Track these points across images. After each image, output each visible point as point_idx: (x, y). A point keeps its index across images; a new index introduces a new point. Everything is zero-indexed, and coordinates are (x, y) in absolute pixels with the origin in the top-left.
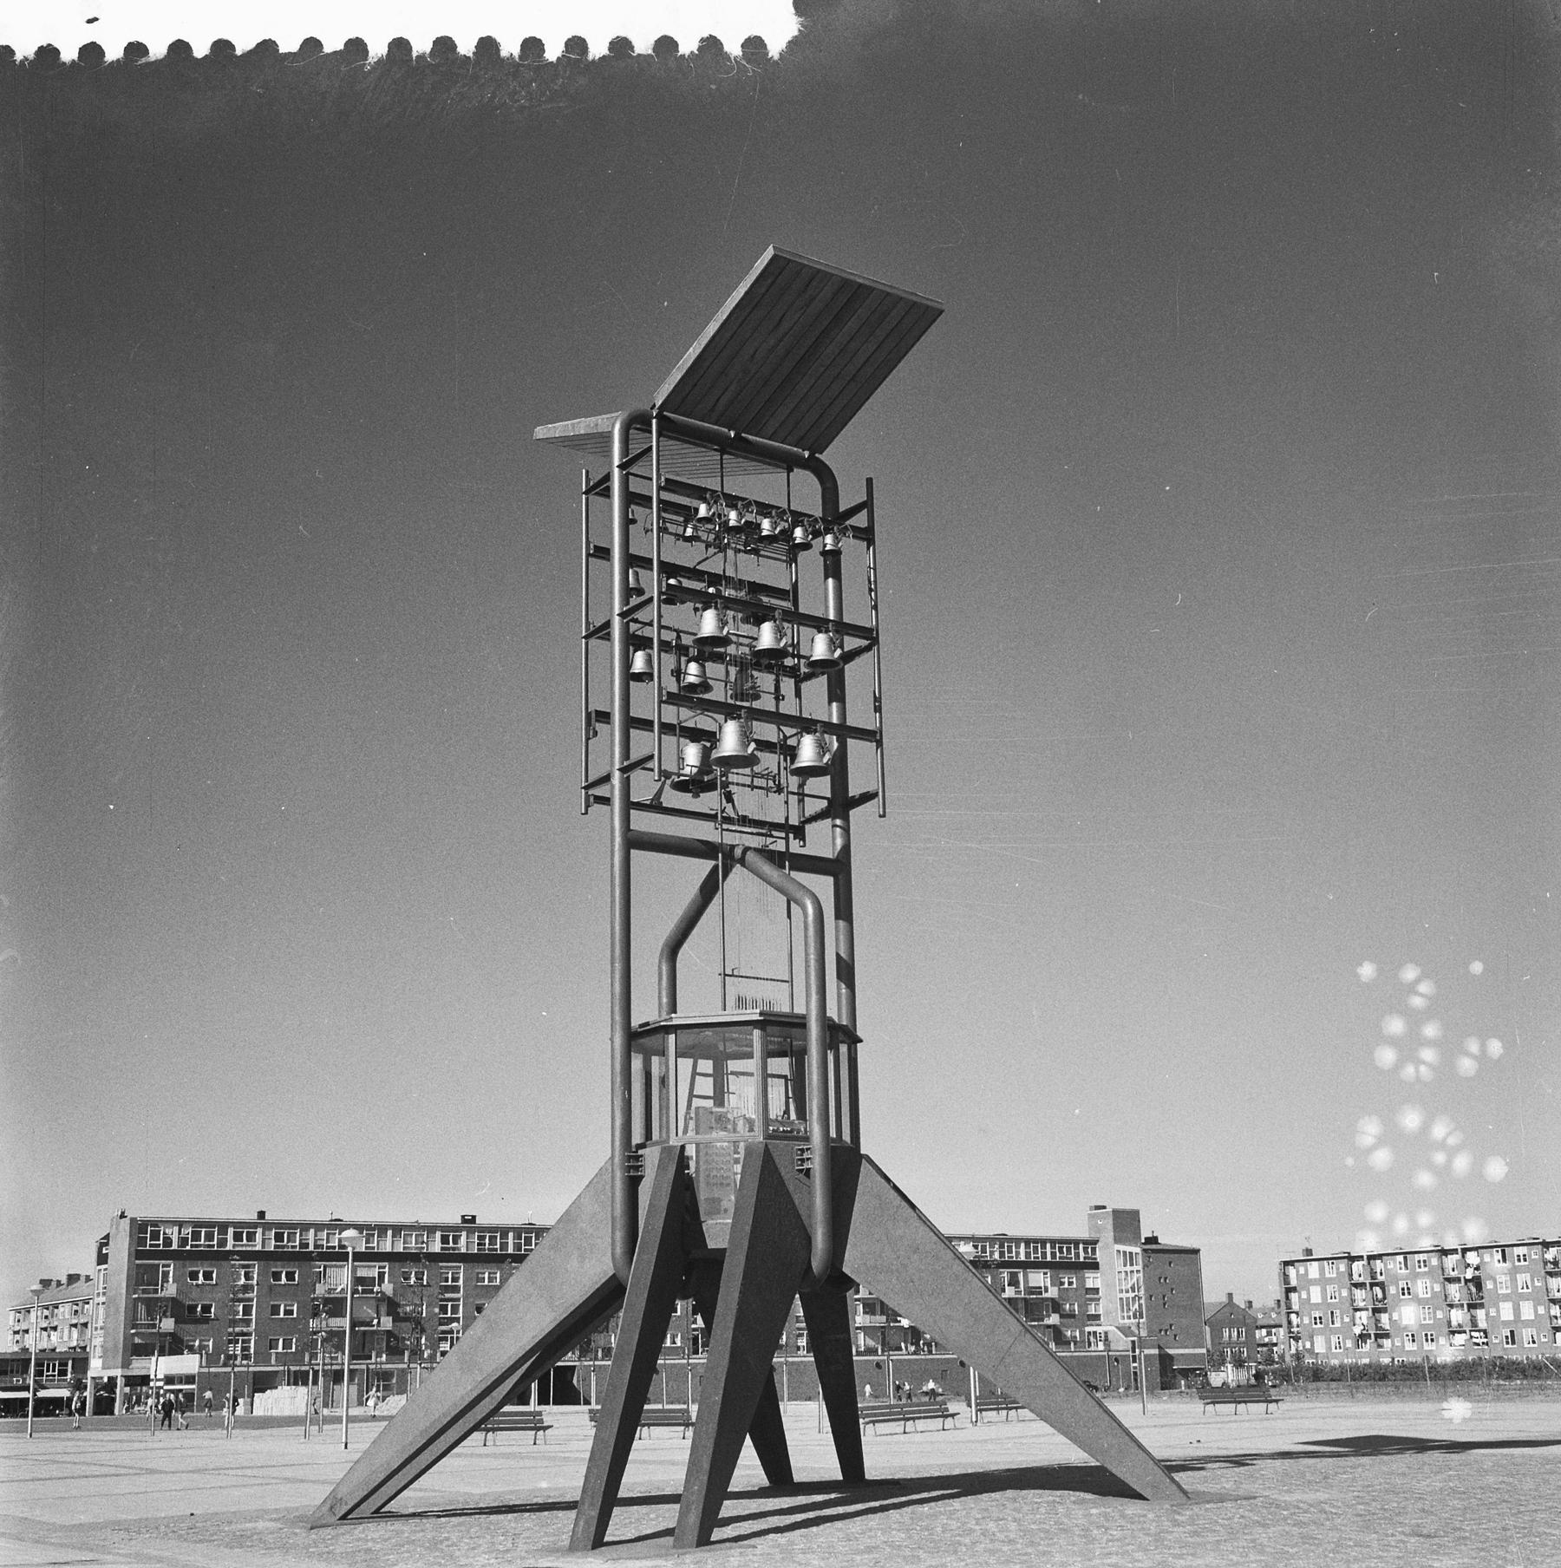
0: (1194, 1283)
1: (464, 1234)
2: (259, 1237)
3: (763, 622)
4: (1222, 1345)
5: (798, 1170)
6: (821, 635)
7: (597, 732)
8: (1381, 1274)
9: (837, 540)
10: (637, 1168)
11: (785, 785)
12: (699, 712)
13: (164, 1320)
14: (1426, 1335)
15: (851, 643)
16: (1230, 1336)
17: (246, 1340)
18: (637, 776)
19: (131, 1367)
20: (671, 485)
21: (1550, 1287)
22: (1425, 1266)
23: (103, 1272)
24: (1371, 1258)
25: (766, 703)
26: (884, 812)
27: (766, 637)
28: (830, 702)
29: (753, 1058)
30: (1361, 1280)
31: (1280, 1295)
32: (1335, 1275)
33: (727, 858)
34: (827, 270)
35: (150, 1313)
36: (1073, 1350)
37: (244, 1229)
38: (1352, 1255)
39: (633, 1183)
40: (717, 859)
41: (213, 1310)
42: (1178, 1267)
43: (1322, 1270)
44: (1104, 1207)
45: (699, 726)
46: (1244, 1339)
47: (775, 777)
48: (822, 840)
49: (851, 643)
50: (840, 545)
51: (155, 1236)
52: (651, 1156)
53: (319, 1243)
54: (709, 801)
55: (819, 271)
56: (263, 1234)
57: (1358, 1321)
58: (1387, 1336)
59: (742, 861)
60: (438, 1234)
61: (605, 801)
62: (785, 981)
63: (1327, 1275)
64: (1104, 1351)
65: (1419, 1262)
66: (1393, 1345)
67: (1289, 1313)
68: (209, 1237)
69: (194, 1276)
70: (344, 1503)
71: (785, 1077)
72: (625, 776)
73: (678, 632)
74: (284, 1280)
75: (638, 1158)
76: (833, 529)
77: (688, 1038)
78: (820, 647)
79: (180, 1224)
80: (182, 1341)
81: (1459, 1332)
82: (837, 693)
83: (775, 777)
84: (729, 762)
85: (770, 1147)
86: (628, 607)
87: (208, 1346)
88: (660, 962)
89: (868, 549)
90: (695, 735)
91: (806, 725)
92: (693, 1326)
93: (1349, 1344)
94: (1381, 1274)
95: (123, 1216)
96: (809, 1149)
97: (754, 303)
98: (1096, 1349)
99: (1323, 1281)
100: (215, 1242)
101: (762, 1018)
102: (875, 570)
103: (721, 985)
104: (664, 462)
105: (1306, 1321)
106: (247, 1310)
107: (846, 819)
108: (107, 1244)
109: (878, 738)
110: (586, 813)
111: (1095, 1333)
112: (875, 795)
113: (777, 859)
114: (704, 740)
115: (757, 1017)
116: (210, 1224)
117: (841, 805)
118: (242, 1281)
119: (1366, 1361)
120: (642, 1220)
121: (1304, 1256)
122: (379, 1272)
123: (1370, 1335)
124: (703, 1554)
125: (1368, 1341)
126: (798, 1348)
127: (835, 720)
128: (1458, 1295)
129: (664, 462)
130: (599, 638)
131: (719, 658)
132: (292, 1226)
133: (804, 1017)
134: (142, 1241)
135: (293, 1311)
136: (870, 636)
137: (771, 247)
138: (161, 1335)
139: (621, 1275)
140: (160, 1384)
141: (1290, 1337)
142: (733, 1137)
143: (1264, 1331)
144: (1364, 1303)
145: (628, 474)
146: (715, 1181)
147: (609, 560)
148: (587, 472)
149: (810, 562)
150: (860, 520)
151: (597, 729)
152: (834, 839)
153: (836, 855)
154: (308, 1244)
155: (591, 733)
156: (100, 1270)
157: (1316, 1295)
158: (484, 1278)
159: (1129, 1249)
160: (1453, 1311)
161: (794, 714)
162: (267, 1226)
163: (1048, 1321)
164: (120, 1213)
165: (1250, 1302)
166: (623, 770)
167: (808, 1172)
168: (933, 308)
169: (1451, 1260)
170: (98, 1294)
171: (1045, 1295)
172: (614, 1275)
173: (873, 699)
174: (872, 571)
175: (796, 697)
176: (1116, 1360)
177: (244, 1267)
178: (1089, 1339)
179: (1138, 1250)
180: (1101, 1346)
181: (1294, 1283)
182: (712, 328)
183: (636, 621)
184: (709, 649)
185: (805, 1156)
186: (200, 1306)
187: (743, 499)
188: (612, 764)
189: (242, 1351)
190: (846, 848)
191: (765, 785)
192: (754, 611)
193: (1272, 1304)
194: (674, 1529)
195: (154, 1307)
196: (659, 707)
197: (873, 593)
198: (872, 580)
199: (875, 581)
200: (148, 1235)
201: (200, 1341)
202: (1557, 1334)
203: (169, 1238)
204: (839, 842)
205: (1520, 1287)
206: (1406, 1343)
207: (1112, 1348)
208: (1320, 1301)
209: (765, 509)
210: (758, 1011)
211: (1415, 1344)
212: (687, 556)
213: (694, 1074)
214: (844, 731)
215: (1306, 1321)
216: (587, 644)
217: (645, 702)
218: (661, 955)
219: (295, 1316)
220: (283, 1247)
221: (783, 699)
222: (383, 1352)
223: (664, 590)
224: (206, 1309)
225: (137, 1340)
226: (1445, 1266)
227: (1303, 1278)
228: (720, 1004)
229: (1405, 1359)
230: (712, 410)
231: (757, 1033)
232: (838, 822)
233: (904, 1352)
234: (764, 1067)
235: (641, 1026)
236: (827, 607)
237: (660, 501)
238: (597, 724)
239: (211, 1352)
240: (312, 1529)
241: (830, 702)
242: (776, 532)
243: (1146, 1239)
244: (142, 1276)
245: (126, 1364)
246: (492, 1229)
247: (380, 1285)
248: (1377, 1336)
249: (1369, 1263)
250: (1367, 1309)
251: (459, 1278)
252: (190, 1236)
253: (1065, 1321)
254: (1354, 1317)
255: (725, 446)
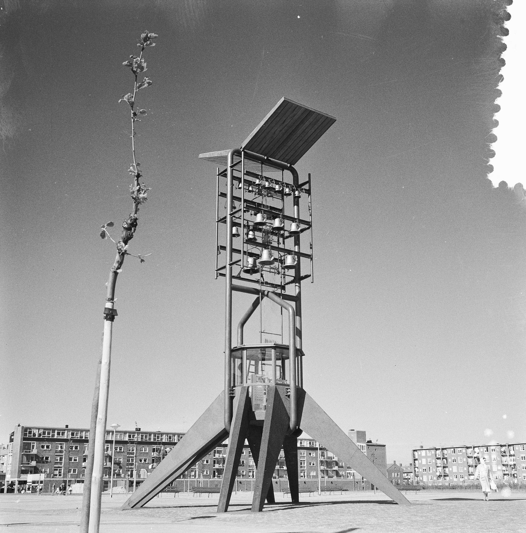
0: (384, 457)
1: (136, 434)
2: (66, 434)
3: (276, 218)
4: (392, 479)
5: (286, 395)
6: (294, 223)
7: (220, 253)
8: (446, 455)
9: (299, 193)
10: (233, 394)
11: (281, 272)
12: (254, 246)
13: (32, 462)
14: (461, 476)
15: (303, 226)
16: (394, 475)
17: (61, 469)
18: (234, 266)
19: (20, 477)
20: (248, 173)
21: (503, 460)
22: (461, 452)
23: (11, 445)
24: (443, 449)
25: (275, 244)
26: (313, 281)
27: (277, 223)
28: (295, 246)
29: (271, 360)
30: (439, 457)
31: (412, 462)
32: (431, 455)
33: (262, 294)
34: (301, 106)
35: (28, 460)
36: (342, 478)
37: (61, 431)
38: (437, 448)
39: (231, 398)
40: (259, 295)
41: (49, 459)
42: (379, 450)
43: (426, 454)
44: (354, 430)
45: (252, 252)
46: (399, 477)
47: (277, 269)
48: (291, 290)
49: (303, 226)
50: (300, 195)
51: (30, 433)
52: (238, 390)
53: (86, 436)
54: (256, 276)
55: (298, 106)
56: (67, 433)
57: (438, 471)
58: (448, 476)
59: (267, 296)
60: (128, 434)
61: (224, 275)
62: (280, 335)
63: (428, 455)
64: (353, 479)
65: (459, 451)
66: (449, 479)
67: (415, 468)
68: (49, 434)
69: (43, 447)
70: (133, 502)
71: (280, 366)
72: (231, 266)
73: (248, 221)
74: (74, 449)
75: (233, 390)
76: (298, 189)
77: (250, 352)
78: (293, 227)
79: (39, 429)
80: (38, 469)
81: (472, 475)
82: (297, 242)
83: (277, 269)
84: (264, 263)
85: (277, 387)
86: (232, 212)
87: (47, 471)
88: (238, 328)
89: (309, 196)
90: (251, 255)
91: (289, 252)
92: (214, 468)
93: (435, 478)
94: (446, 455)
95: (19, 426)
96: (290, 388)
97: (276, 116)
98: (350, 478)
99: (426, 457)
100: (51, 435)
101: (275, 346)
102: (311, 203)
103: (259, 337)
104: (245, 166)
105: (421, 470)
106: (61, 459)
107: (300, 283)
108: (13, 435)
109: (311, 257)
110: (217, 279)
111: (350, 473)
112: (310, 276)
113: (279, 295)
114: (254, 257)
115: (273, 345)
116: (50, 429)
117: (298, 279)
118: (60, 449)
119: (441, 484)
120: (235, 412)
121: (420, 448)
122: (107, 447)
123: (442, 475)
124: (261, 513)
125: (441, 477)
126: (249, 476)
127: (296, 251)
128: (471, 462)
129: (245, 166)
130: (221, 222)
131: (260, 230)
132: (77, 430)
133: (288, 346)
134: (26, 435)
135: (77, 460)
136: (309, 224)
137: (283, 97)
138: (31, 467)
139: (227, 428)
140: (31, 484)
141: (415, 476)
142: (264, 384)
143: (406, 474)
144: (440, 465)
145: (233, 169)
146: (258, 398)
147: (226, 197)
148: (219, 168)
149: (290, 200)
150: (306, 187)
151: (220, 252)
152: (296, 290)
153: (296, 294)
154: (83, 437)
155: (219, 253)
156: (11, 444)
157: (424, 461)
158: (143, 450)
159: (362, 444)
160: (470, 468)
161: (282, 248)
162: (69, 430)
163: (334, 469)
164: (18, 425)
165: (401, 464)
166: (230, 265)
167: (289, 396)
168: (333, 119)
169: (470, 450)
170: (10, 452)
171: (333, 460)
172: (225, 428)
173: (310, 245)
174: (310, 203)
175: (283, 244)
176: (357, 482)
177: (60, 444)
178: (348, 475)
179: (365, 445)
180: (352, 478)
181: (417, 457)
182: (262, 123)
183: (234, 217)
184: (257, 227)
185: (288, 391)
186: (45, 457)
187: (270, 179)
188: (226, 263)
189: (59, 473)
190: (300, 293)
191: (274, 272)
192: (273, 214)
193: (409, 465)
194: (251, 508)
195: (30, 458)
196: (243, 245)
197: (310, 211)
198: (310, 206)
199: (311, 207)
200: (28, 433)
201: (45, 469)
202: (505, 476)
203: (35, 434)
204: (297, 291)
205: (492, 460)
206: (454, 478)
207: (355, 478)
208: (425, 464)
209: (277, 182)
210: (273, 343)
211: (457, 479)
212: (250, 197)
213: (250, 365)
214: (299, 254)
215: (421, 470)
216: (218, 224)
217: (238, 243)
218: (239, 325)
219: (77, 461)
220: (74, 438)
221: (280, 244)
222: (107, 474)
223: (245, 207)
224: (47, 458)
225: (23, 469)
226: (468, 452)
227: (420, 456)
228: (259, 341)
229: (454, 484)
230: (260, 149)
231: (273, 350)
232: (297, 284)
233: (285, 478)
234: (275, 362)
235: (234, 348)
236: (294, 214)
237: (244, 180)
238: (221, 250)
239: (48, 473)
240: (123, 510)
241: (295, 246)
242: (281, 190)
243: (367, 441)
244: (26, 446)
245: (19, 477)
246: (146, 433)
247: (107, 451)
248: (445, 476)
249: (442, 451)
250: (441, 467)
251: (134, 450)
252: (42, 433)
253: (339, 468)
254: (437, 470)
255: (263, 162)
